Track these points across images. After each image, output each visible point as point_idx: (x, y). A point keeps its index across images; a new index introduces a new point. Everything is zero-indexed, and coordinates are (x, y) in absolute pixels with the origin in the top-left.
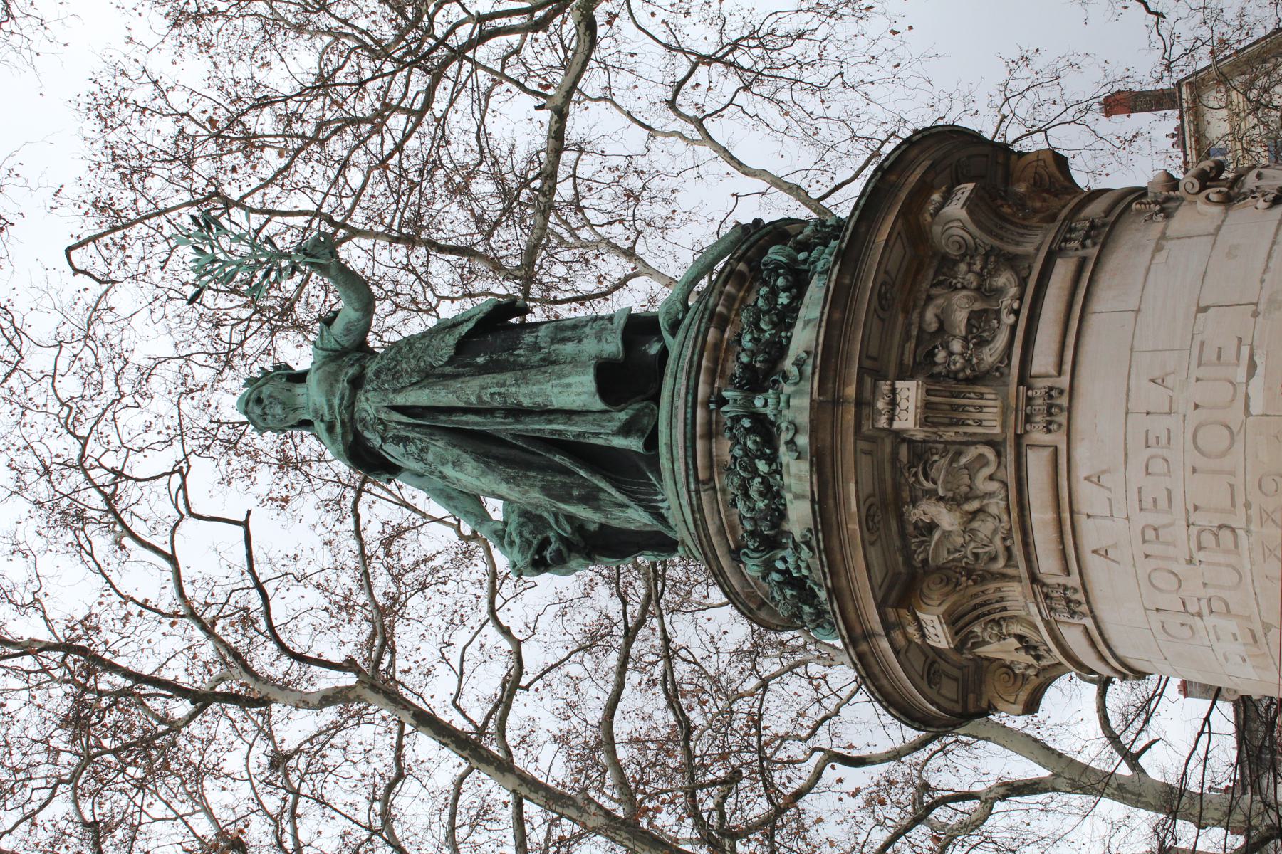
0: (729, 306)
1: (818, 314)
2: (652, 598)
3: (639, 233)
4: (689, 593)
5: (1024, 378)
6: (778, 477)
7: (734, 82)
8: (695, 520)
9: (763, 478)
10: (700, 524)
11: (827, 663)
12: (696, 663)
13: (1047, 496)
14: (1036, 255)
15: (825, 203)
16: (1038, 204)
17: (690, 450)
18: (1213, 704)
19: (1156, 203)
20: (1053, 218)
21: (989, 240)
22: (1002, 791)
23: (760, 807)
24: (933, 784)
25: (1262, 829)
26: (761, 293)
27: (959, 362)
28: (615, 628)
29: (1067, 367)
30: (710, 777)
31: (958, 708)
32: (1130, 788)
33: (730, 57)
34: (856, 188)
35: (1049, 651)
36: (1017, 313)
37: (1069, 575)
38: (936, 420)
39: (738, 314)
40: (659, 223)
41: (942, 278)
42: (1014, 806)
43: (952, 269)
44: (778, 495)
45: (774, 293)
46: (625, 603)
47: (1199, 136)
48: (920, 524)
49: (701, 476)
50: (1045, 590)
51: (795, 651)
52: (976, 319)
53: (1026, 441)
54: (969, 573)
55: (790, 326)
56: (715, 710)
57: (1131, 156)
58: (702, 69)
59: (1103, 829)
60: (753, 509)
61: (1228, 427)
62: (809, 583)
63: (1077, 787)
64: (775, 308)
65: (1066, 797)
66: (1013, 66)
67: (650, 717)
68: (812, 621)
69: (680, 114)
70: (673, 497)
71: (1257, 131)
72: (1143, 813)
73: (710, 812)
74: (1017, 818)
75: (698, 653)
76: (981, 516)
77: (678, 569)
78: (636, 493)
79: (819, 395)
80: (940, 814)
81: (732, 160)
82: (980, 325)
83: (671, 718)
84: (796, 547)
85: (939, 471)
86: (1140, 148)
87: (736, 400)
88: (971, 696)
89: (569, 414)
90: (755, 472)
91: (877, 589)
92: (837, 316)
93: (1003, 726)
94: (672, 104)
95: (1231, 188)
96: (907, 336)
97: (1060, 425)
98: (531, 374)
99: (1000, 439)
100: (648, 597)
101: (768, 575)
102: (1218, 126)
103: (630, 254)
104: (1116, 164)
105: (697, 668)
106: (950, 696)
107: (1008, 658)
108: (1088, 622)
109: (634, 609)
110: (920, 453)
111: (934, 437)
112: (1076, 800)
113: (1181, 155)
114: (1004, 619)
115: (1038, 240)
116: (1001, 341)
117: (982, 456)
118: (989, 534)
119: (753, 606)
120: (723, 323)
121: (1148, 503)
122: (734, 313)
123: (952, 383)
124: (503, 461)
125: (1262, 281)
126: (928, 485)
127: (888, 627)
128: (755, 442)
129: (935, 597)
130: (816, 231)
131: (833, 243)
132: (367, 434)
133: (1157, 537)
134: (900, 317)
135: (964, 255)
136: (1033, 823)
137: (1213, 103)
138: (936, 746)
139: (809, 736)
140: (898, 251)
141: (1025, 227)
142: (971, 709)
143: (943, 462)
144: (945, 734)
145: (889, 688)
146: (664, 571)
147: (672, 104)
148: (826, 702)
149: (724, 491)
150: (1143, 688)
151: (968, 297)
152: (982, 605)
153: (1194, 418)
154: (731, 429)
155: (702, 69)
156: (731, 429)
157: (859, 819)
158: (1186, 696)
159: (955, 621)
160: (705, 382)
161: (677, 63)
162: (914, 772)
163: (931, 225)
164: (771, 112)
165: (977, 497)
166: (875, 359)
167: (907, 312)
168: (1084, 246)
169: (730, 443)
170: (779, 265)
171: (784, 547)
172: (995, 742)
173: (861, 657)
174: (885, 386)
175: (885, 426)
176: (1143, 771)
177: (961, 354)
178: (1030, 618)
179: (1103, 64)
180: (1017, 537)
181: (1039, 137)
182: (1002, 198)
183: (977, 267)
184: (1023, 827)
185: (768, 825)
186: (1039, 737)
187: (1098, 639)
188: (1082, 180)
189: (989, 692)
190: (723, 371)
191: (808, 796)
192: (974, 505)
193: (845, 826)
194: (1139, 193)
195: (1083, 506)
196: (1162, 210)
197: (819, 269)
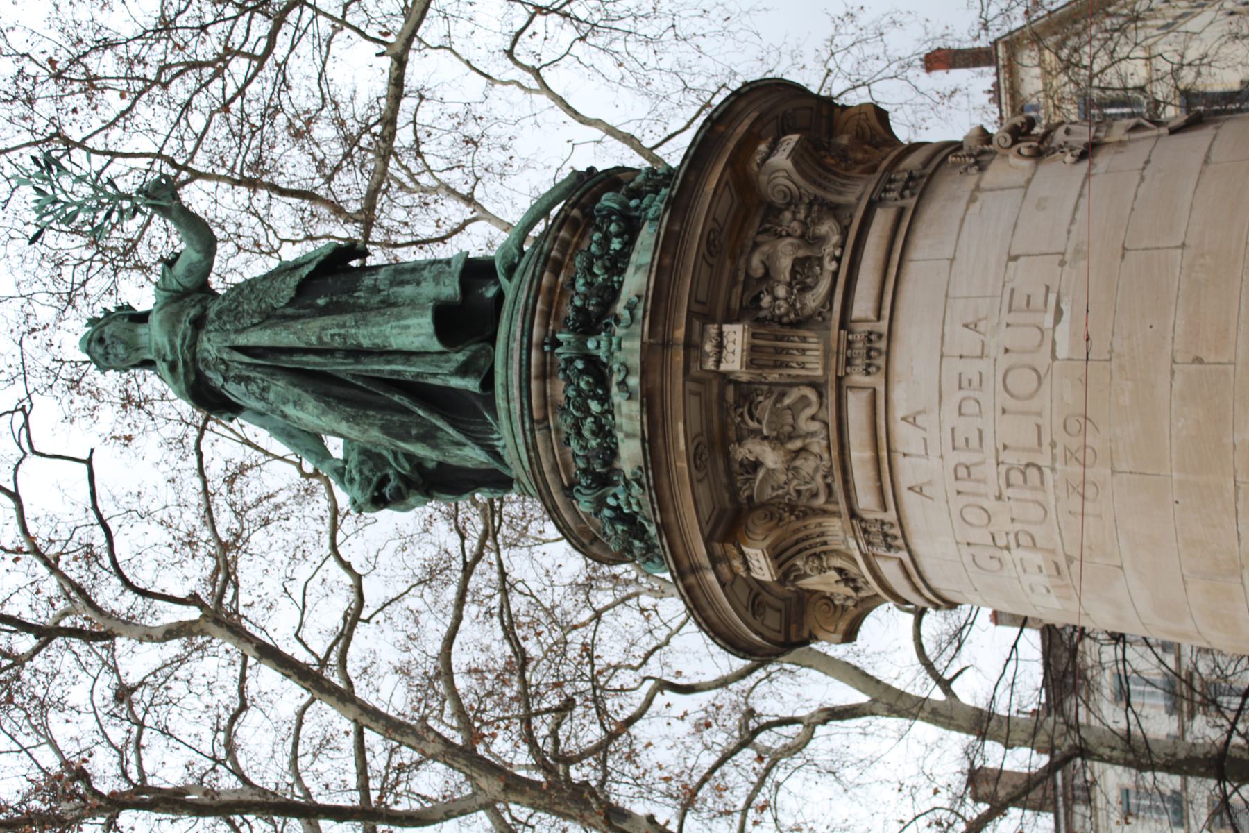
0: (563, 251)
1: (649, 260)
2: (489, 533)
3: (478, 179)
4: (526, 528)
5: (845, 323)
6: (610, 417)
7: (570, 32)
10: (535, 462)
13: (866, 435)
16: (860, 156)
18: (1021, 631)
19: (971, 156)
20: (873, 169)
21: (813, 190)
22: (823, 715)
23: (594, 734)
24: (758, 710)
25: (1065, 749)
26: (595, 238)
27: (783, 307)
28: (453, 563)
29: (886, 312)
30: (545, 705)
31: (781, 638)
33: (567, 9)
34: (686, 139)
35: (867, 583)
36: (838, 260)
38: (761, 362)
39: (572, 259)
41: (768, 226)
42: (835, 730)
44: (610, 434)
45: (607, 239)
46: (463, 538)
47: (1014, 92)
48: (746, 462)
49: (536, 415)
50: (863, 525)
52: (801, 266)
53: (847, 382)
54: (792, 508)
55: (622, 271)
56: (550, 641)
59: (919, 750)
61: (1035, 370)
62: (639, 518)
63: (893, 711)
64: (607, 253)
65: (882, 721)
66: (838, 22)
67: (488, 648)
68: (643, 555)
69: (517, 63)
70: (509, 437)
71: (1067, 89)
72: (955, 735)
73: (545, 737)
74: (837, 741)
75: (534, 587)
76: (803, 454)
77: (516, 505)
79: (650, 337)
80: (764, 739)
81: (568, 108)
82: (803, 270)
83: (508, 650)
84: (627, 485)
85: (763, 410)
86: (958, 104)
88: (793, 627)
89: (407, 355)
90: (587, 411)
91: (704, 524)
92: (667, 261)
93: (825, 655)
94: (510, 53)
95: (1041, 142)
96: (734, 281)
97: (878, 368)
98: (371, 316)
99: (822, 381)
102: (1031, 83)
105: (533, 601)
107: (828, 590)
108: (904, 555)
109: (472, 544)
110: (746, 394)
112: (894, 723)
113: (997, 110)
114: (825, 553)
115: (858, 190)
117: (804, 397)
119: (586, 541)
120: (557, 267)
121: (960, 442)
123: (777, 327)
124: (342, 400)
125: (1069, 232)
128: (588, 383)
129: (759, 532)
130: (647, 179)
131: (664, 191)
132: (209, 374)
133: (969, 475)
134: (728, 264)
135: (789, 204)
136: (852, 747)
137: (1027, 61)
138: (760, 673)
139: (641, 665)
140: (726, 197)
141: (848, 178)
142: (794, 639)
143: (768, 403)
145: (714, 619)
146: (501, 507)
147: (510, 53)
149: (558, 430)
150: (955, 617)
151: (792, 244)
152: (803, 540)
153: (1004, 361)
154: (564, 370)
156: (564, 370)
158: (996, 624)
159: (778, 555)
160: (539, 325)
161: (515, 13)
163: (757, 175)
164: (606, 63)
165: (799, 436)
166: (703, 304)
167: (734, 258)
169: (564, 384)
170: (611, 211)
171: (615, 484)
172: (817, 669)
173: (689, 589)
174: (712, 330)
175: (713, 368)
176: (954, 695)
177: (786, 299)
178: (849, 552)
179: (923, 22)
180: (838, 475)
181: (863, 91)
182: (827, 150)
183: (801, 216)
186: (858, 665)
187: (913, 571)
188: (903, 133)
190: (557, 314)
191: (639, 723)
192: (797, 444)
195: (899, 445)
196: (977, 163)
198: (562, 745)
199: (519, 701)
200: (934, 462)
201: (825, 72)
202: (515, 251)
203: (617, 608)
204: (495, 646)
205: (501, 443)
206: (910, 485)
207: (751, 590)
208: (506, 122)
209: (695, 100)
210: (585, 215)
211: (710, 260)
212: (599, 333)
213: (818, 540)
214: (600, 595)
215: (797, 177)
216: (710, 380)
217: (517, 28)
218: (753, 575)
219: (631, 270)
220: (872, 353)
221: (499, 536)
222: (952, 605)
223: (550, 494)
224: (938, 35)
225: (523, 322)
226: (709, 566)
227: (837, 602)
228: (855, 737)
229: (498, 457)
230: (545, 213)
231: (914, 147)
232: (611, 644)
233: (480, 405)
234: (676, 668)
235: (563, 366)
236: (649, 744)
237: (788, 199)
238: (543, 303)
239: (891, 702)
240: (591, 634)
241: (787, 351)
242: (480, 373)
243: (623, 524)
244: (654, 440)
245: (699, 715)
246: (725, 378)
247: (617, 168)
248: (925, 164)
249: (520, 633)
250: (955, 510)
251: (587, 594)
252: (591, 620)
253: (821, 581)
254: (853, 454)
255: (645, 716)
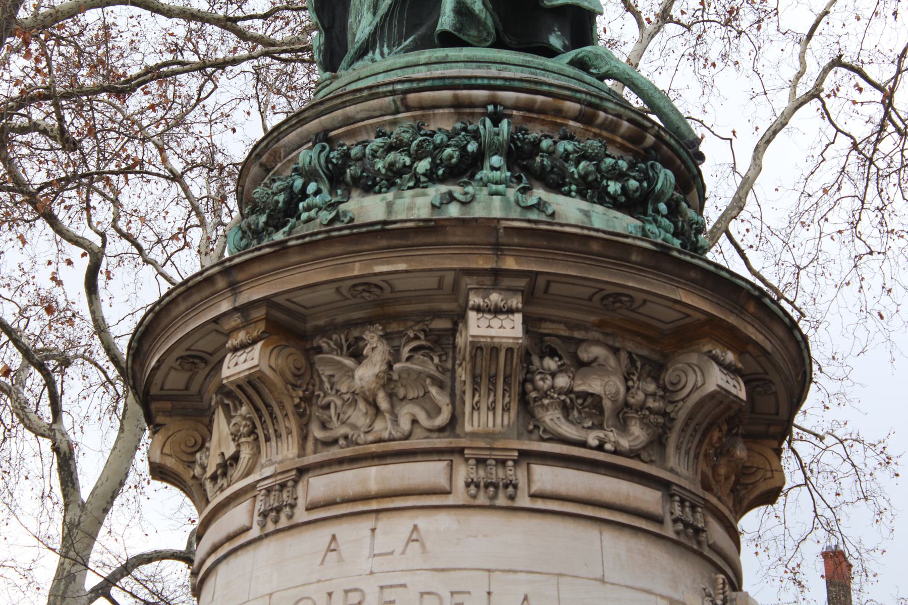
0: (602, 126)
1: (596, 226)
2: (270, 48)
3: (689, 28)
4: (279, 92)
5: (526, 456)
6: (411, 184)
7: (862, 131)
8: (360, 90)
9: (410, 167)
10: (356, 96)
11: (203, 250)
12: (199, 100)
14: (666, 469)
15: (723, 239)
16: (722, 471)
17: (441, 83)
20: (706, 487)
21: (682, 416)
22: (64, 447)
23: (35, 175)
26: (620, 162)
27: (544, 384)
28: (235, 6)
29: (540, 504)
30: (68, 118)
31: (154, 390)
32: (71, 587)
33: (890, 128)
34: (738, 267)
35: (222, 489)
36: (600, 448)
37: (308, 509)
38: (479, 359)
39: (596, 136)
40: (700, 50)
41: (639, 364)
42: (47, 461)
43: (649, 376)
44: (391, 185)
45: (620, 176)
46: (265, 17)
48: (361, 344)
49: (411, 96)
50: (290, 484)
51: (216, 212)
52: (593, 403)
53: (457, 460)
54: (308, 399)
55: (582, 195)
56: (145, 123)
57: (777, 579)
58: (879, 96)
59: (24, 561)
60: (374, 156)
62: (292, 221)
63: (70, 529)
64: (603, 177)
65: (59, 517)
66: (880, 448)
67: (136, 49)
68: (249, 226)
69: (825, 71)
70: (386, 65)
73: (28, 116)
74: (33, 465)
75: (210, 103)
76: (372, 411)
77: (305, 80)
78: (390, 24)
79: (505, 228)
80: (35, 379)
81: (773, 133)
82: (588, 407)
83: (134, 71)
84: (332, 206)
85: (422, 363)
87: (498, 134)
88: (168, 405)
91: (287, 296)
92: (595, 247)
93: (137, 448)
94: (837, 62)
96: (572, 325)
97: (474, 497)
99: (458, 430)
100: (273, 44)
101: (300, 174)
103: (665, 17)
104: (768, 563)
105: (193, 102)
106: (167, 383)
107: (213, 444)
108: (255, 532)
109: (258, 27)
110: (441, 343)
111: (459, 357)
112: (56, 530)
114: (257, 439)
116: (568, 430)
117: (439, 411)
118: (352, 420)
119: (264, 158)
120: (586, 119)
122: (597, 131)
123: (521, 377)
126: (405, 352)
127: (244, 310)
128: (451, 157)
130: (691, 223)
131: (677, 243)
134: (593, 318)
135: (665, 389)
138: (113, 373)
139: (119, 231)
140: (670, 315)
141: (696, 457)
142: (154, 406)
143: (431, 369)
144: (126, 383)
145: (175, 311)
146: (303, 61)
147: (837, 62)
148: (158, 249)
149: (394, 123)
150: (183, 598)
151: (617, 393)
154: (465, 129)
155: (879, 96)
156: (465, 129)
157: (26, 289)
159: (253, 384)
160: (518, 99)
161: (885, 66)
162: (82, 350)
163: (698, 351)
164: (827, 174)
165: (392, 406)
166: (546, 291)
167: (600, 325)
168: (675, 521)
169: (449, 129)
170: (652, 181)
171: (332, 192)
173: (210, 280)
174: (516, 302)
175: (471, 303)
177: (553, 387)
179: (881, 547)
180: (348, 452)
181: (799, 478)
182: (729, 431)
183: (651, 403)
184: (24, 472)
185: (19, 185)
186: (126, 487)
187: (237, 544)
188: (750, 522)
189: (173, 425)
190: (531, 120)
191: (50, 230)
192: (384, 404)
193: (17, 273)
194: (735, 582)
195: (384, 523)
197: (648, 227)
198: (19, 138)
199: (72, 86)
200: (366, 565)
201: (821, 433)
202: (603, 70)
203: (187, 202)
204: (137, 57)
205: (377, 56)
206: (338, 537)
207: (211, 355)
208: (756, 59)
209: (784, 281)
210: (647, 150)
211: (597, 298)
212: (509, 170)
213: (271, 431)
214: (201, 181)
215: (696, 397)
216: (456, 300)
217: (867, 69)
218: (229, 356)
219: (584, 205)
220: (492, 489)
221: (268, 60)
222: (197, 591)
223: (318, 116)
224: (866, 565)
225: (521, 80)
226: (237, 305)
227: (198, 455)
228: (39, 486)
229: (362, 52)
230: (654, 109)
231: (735, 535)
232: (143, 195)
233: (422, 31)
234: (117, 272)
235: (470, 127)
236: (24, 242)
237: (670, 388)
238: (543, 102)
239: (80, 529)
240: (155, 170)
241: (492, 389)
242: (459, 30)
243: (284, 202)
244: (385, 235)
245: (61, 300)
246: (459, 318)
247: (703, 188)
248: (713, 548)
249: (153, 86)
250: (309, 591)
251: (203, 165)
252: (171, 171)
253: (222, 436)
254: (373, 470)
255: (58, 237)
